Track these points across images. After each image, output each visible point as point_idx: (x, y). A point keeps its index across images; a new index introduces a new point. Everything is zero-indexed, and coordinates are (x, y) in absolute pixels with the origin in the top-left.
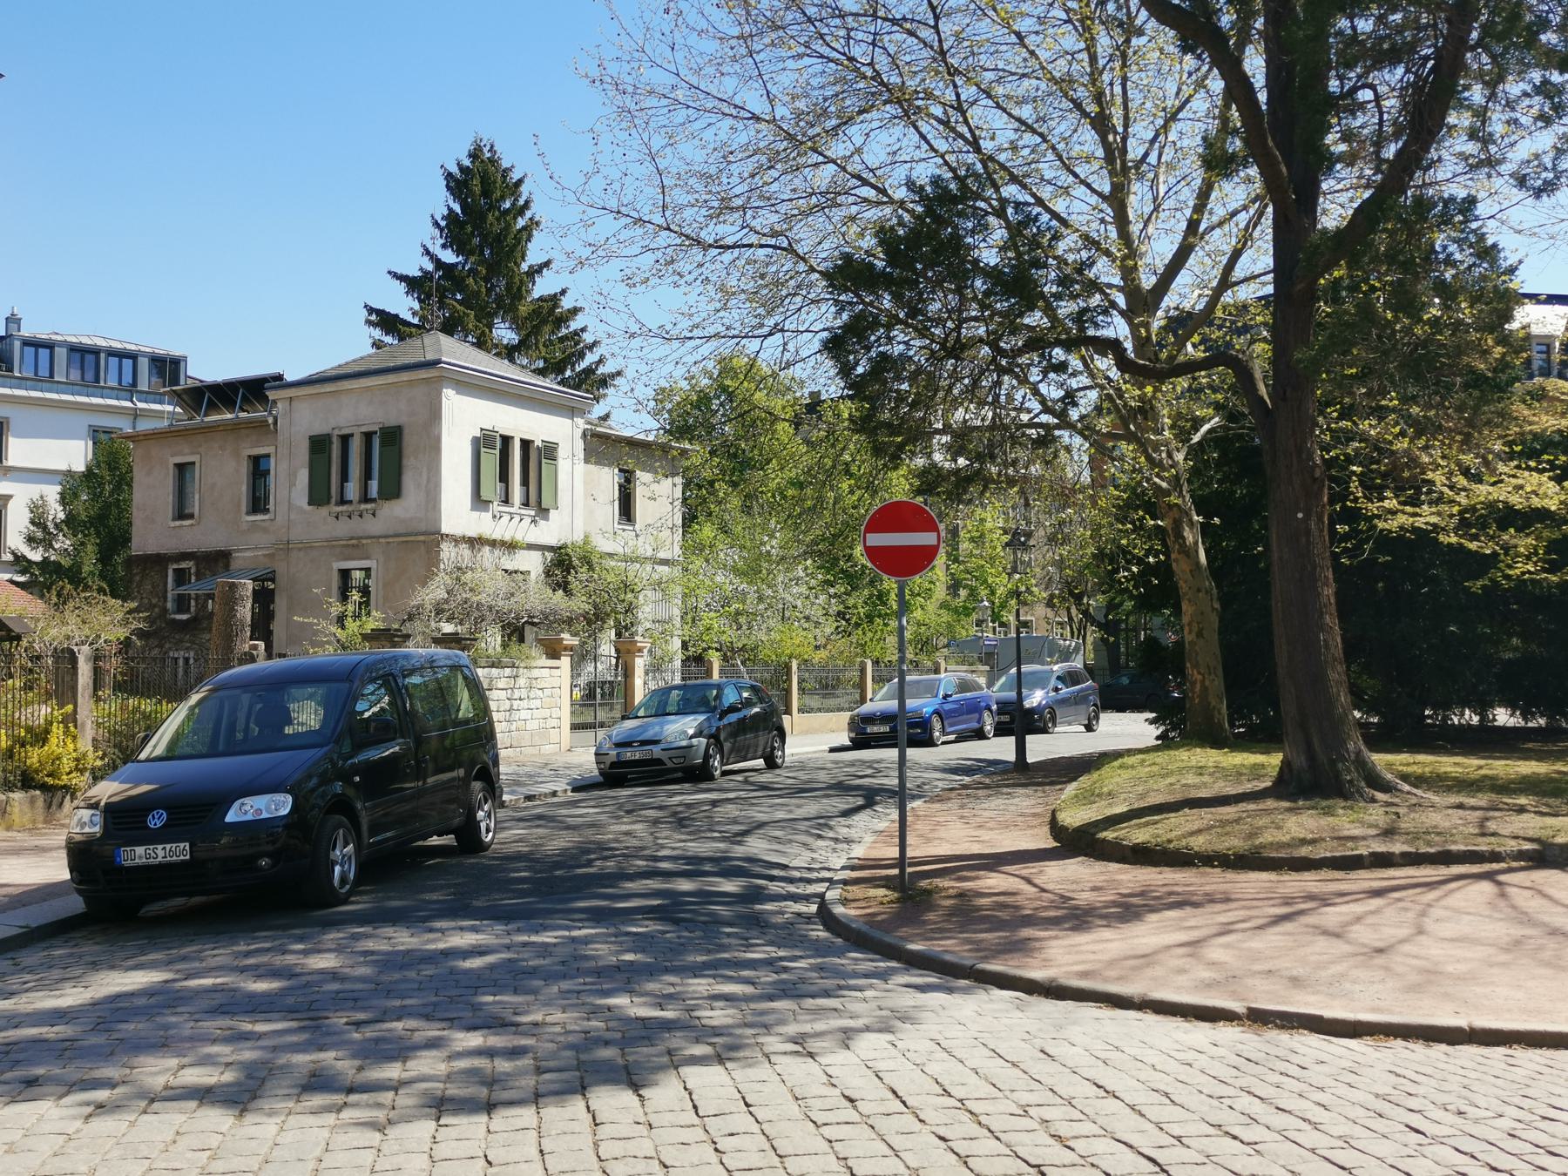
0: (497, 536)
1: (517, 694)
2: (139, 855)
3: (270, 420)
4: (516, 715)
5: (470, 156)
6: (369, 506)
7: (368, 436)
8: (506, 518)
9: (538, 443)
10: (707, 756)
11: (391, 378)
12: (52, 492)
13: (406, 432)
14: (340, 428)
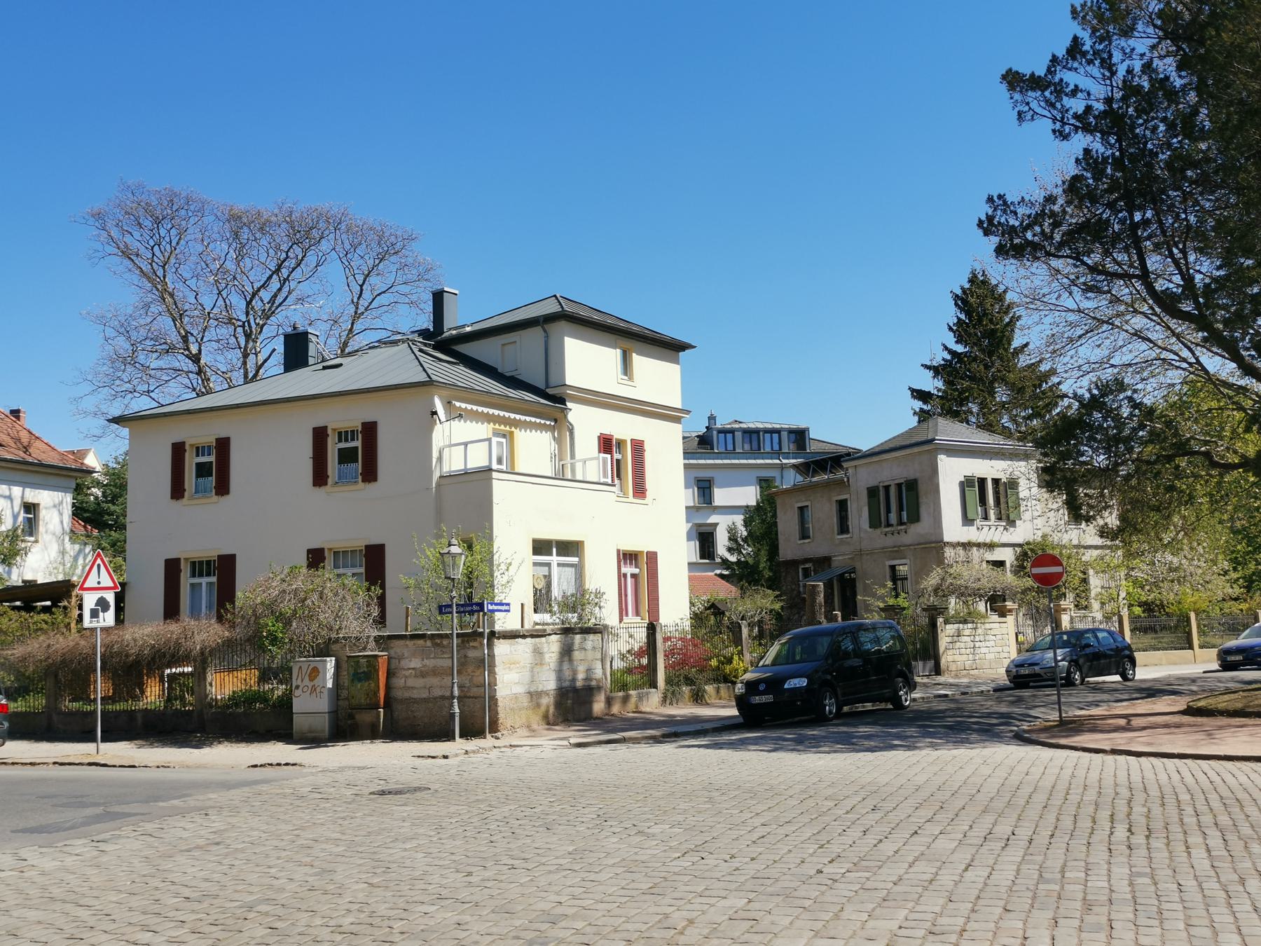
0: (981, 540)
1: (977, 638)
2: (757, 699)
3: (846, 480)
4: (977, 651)
5: (969, 281)
6: (903, 527)
7: (899, 486)
8: (986, 529)
9: (1004, 480)
10: (1069, 672)
11: (908, 451)
12: (739, 519)
13: (919, 482)
14: (883, 482)
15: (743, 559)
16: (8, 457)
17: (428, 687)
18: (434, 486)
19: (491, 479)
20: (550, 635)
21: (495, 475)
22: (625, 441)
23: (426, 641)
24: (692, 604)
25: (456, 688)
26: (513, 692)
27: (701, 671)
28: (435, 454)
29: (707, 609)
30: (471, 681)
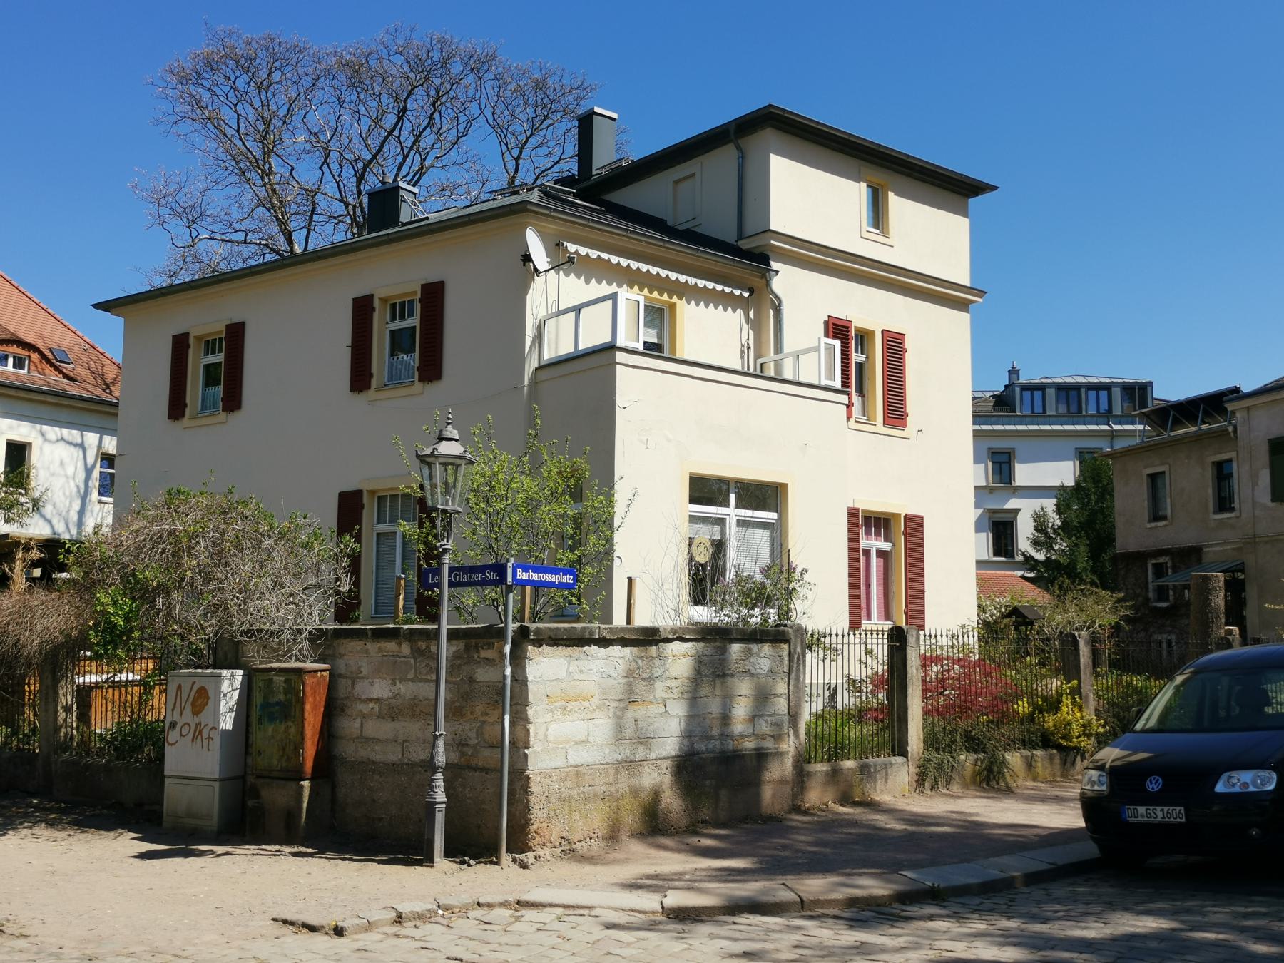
2: (1141, 813)
12: (1050, 504)
15: (1053, 557)
16: (77, 393)
17: (401, 738)
18: (526, 382)
19: (614, 363)
20: (668, 641)
21: (620, 357)
22: (872, 333)
23: (400, 644)
24: (981, 608)
25: (441, 748)
26: (572, 762)
27: (997, 723)
28: (530, 331)
29: (1004, 616)
30: (480, 733)
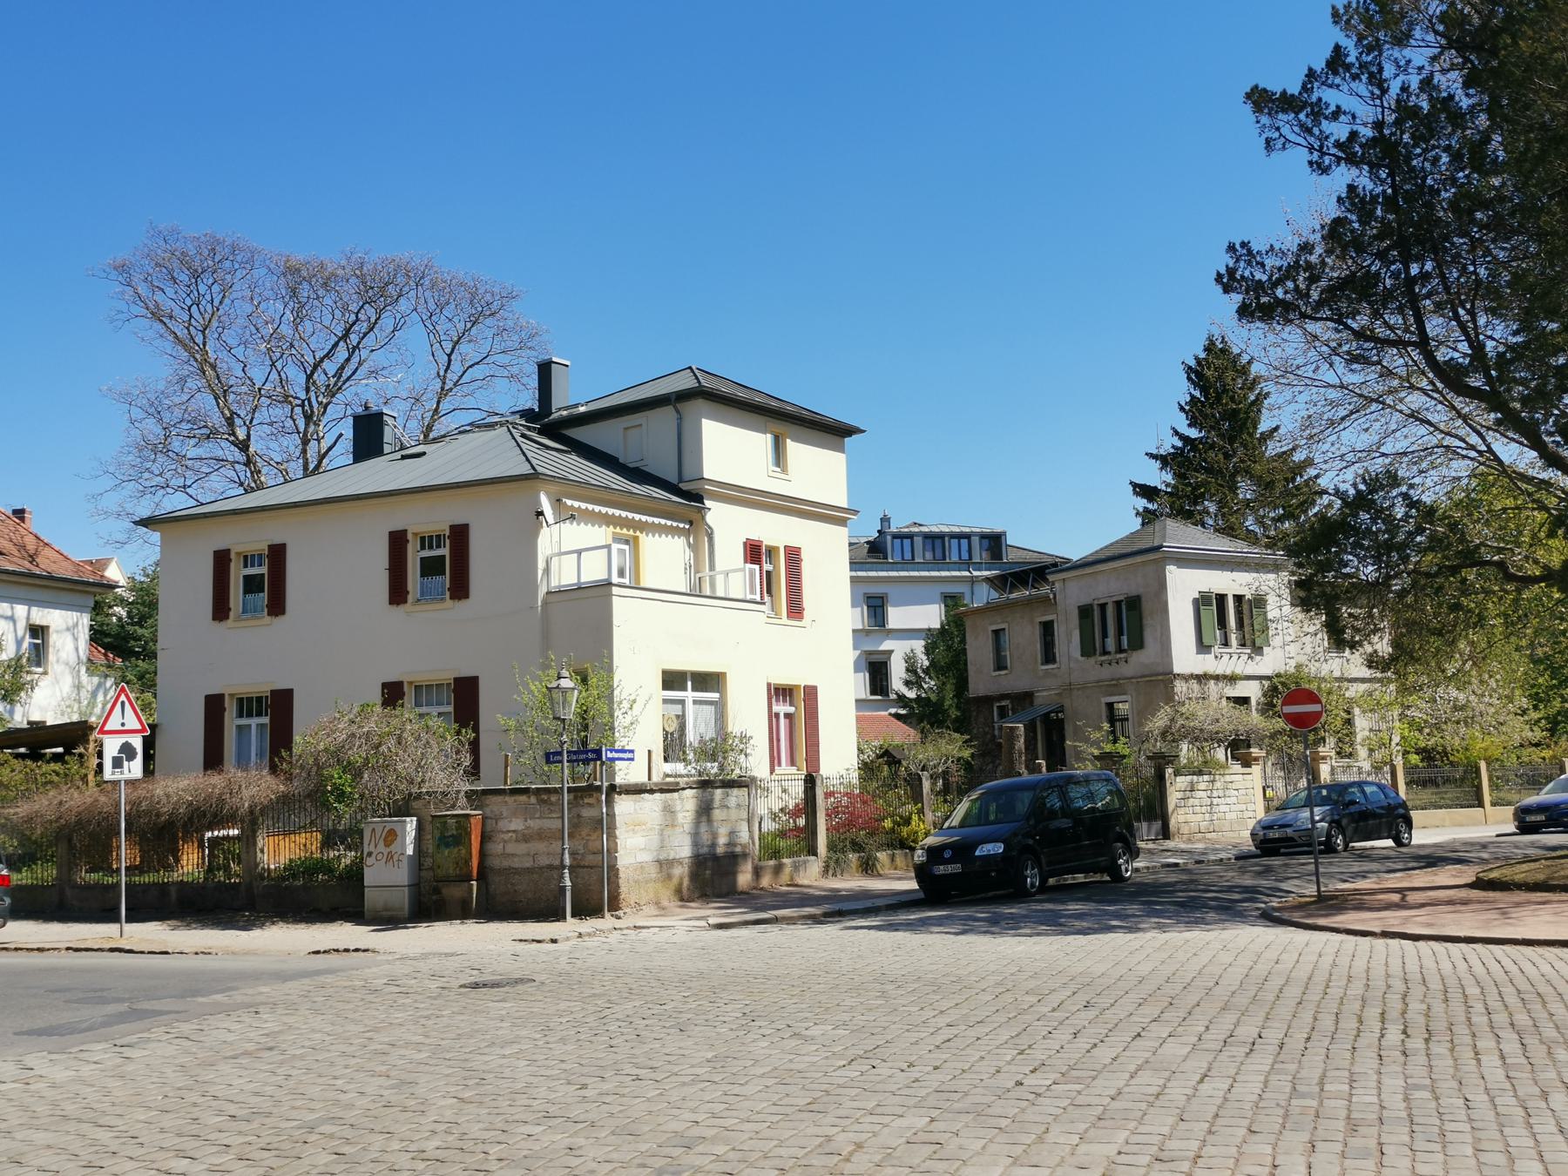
0: (1219, 671)
1: (1215, 794)
2: (941, 870)
3: (1051, 596)
5: (1205, 350)
6: (1122, 655)
7: (1118, 604)
8: (1226, 657)
9: (1249, 596)
10: (1329, 836)
11: (1129, 561)
12: (918, 646)
13: (1143, 599)
14: (1098, 599)
15: (923, 695)
16: (11, 568)
17: (532, 853)
18: (540, 604)
19: (611, 595)
20: (683, 789)
21: (615, 590)
22: (777, 548)
23: (529, 797)
24: (861, 751)
25: (567, 856)
26: (638, 860)
27: (872, 834)
28: (541, 565)
29: (879, 757)
30: (585, 846)
